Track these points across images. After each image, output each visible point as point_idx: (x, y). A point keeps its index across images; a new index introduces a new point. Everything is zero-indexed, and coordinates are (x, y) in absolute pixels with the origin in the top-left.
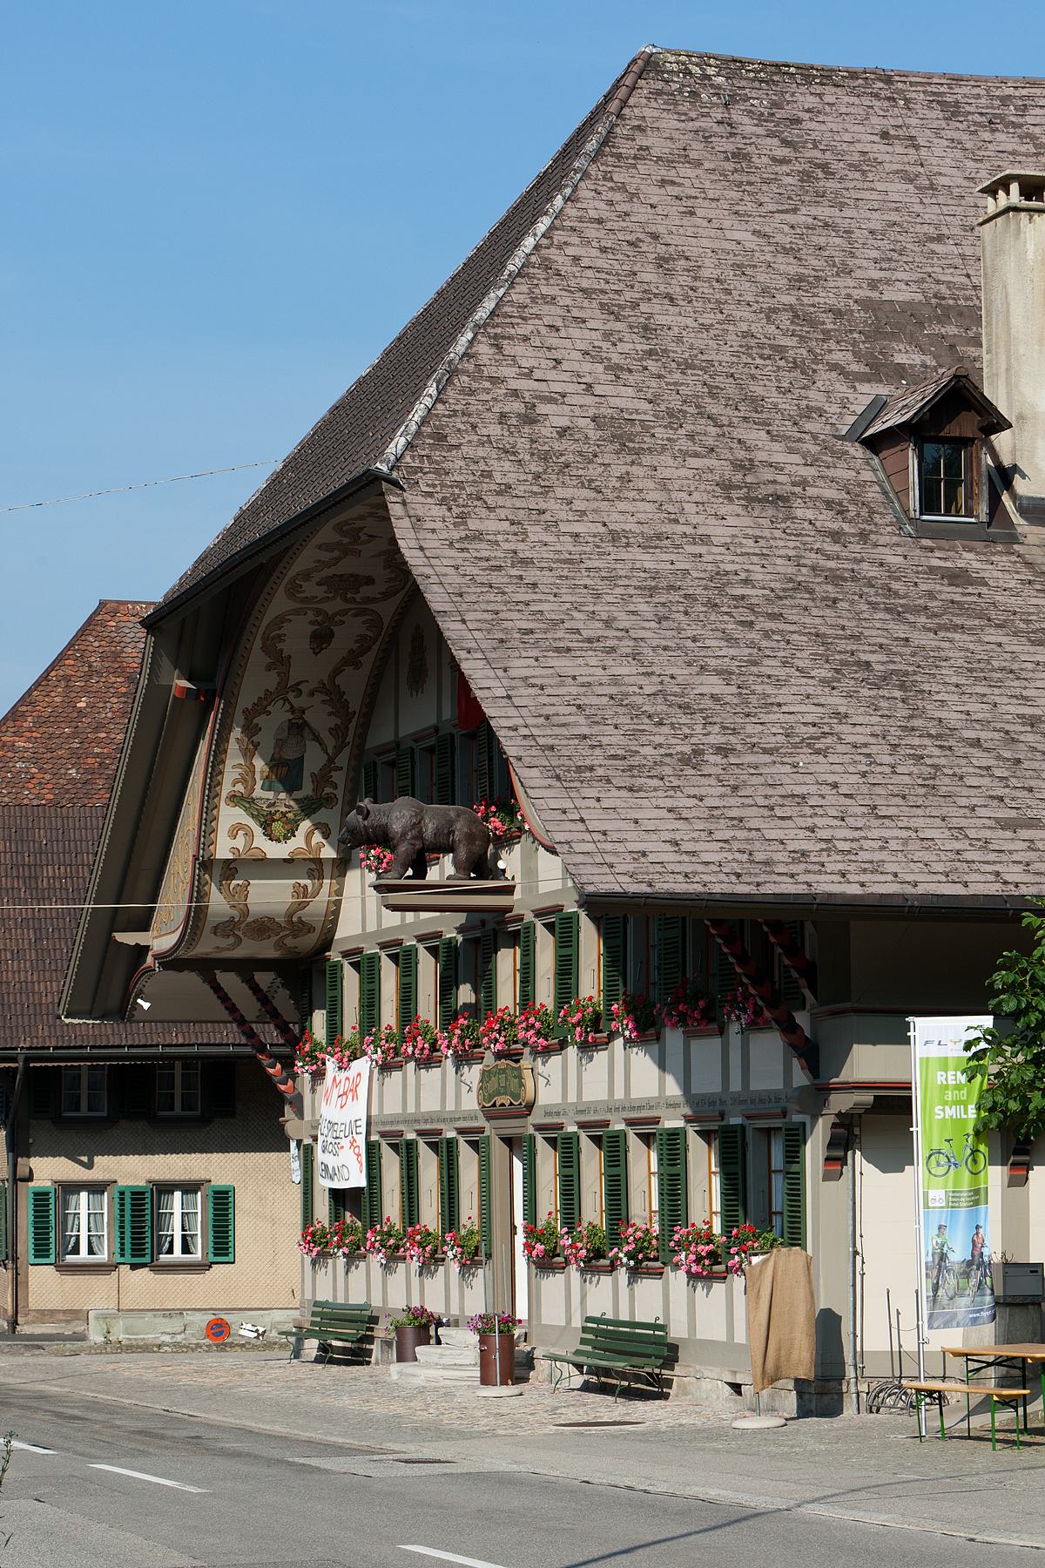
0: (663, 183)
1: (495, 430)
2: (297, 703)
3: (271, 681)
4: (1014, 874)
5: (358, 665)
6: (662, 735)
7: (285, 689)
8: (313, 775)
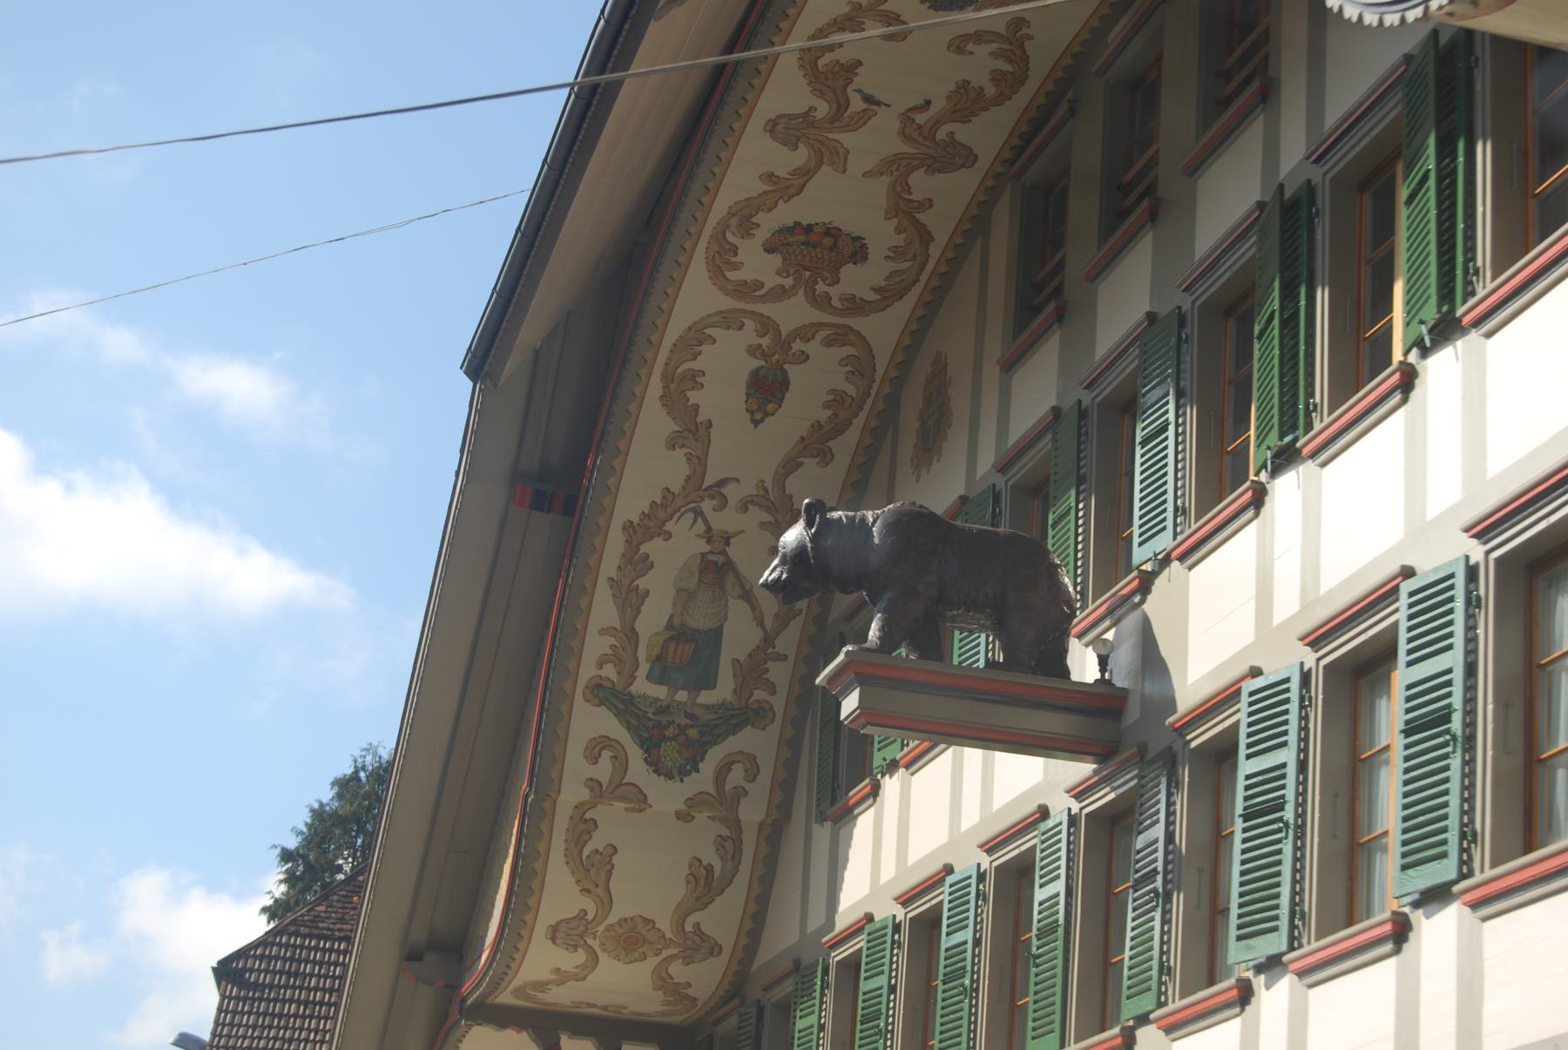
2: (720, 522)
3: (672, 470)
5: (825, 456)
8: (736, 663)
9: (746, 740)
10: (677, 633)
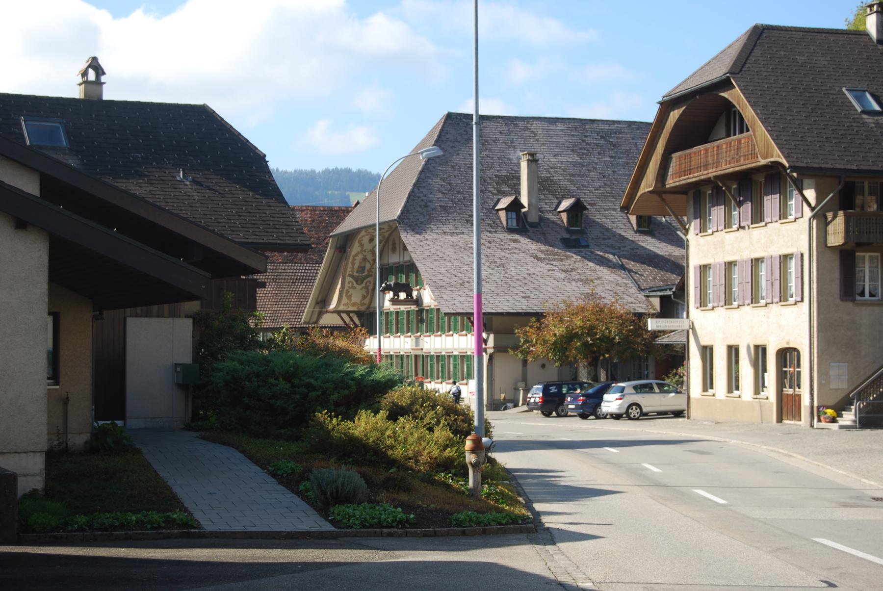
0: (452, 147)
1: (419, 209)
3: (359, 249)
4: (524, 307)
6: (456, 279)
7: (362, 251)
9: (369, 279)
10: (359, 267)
